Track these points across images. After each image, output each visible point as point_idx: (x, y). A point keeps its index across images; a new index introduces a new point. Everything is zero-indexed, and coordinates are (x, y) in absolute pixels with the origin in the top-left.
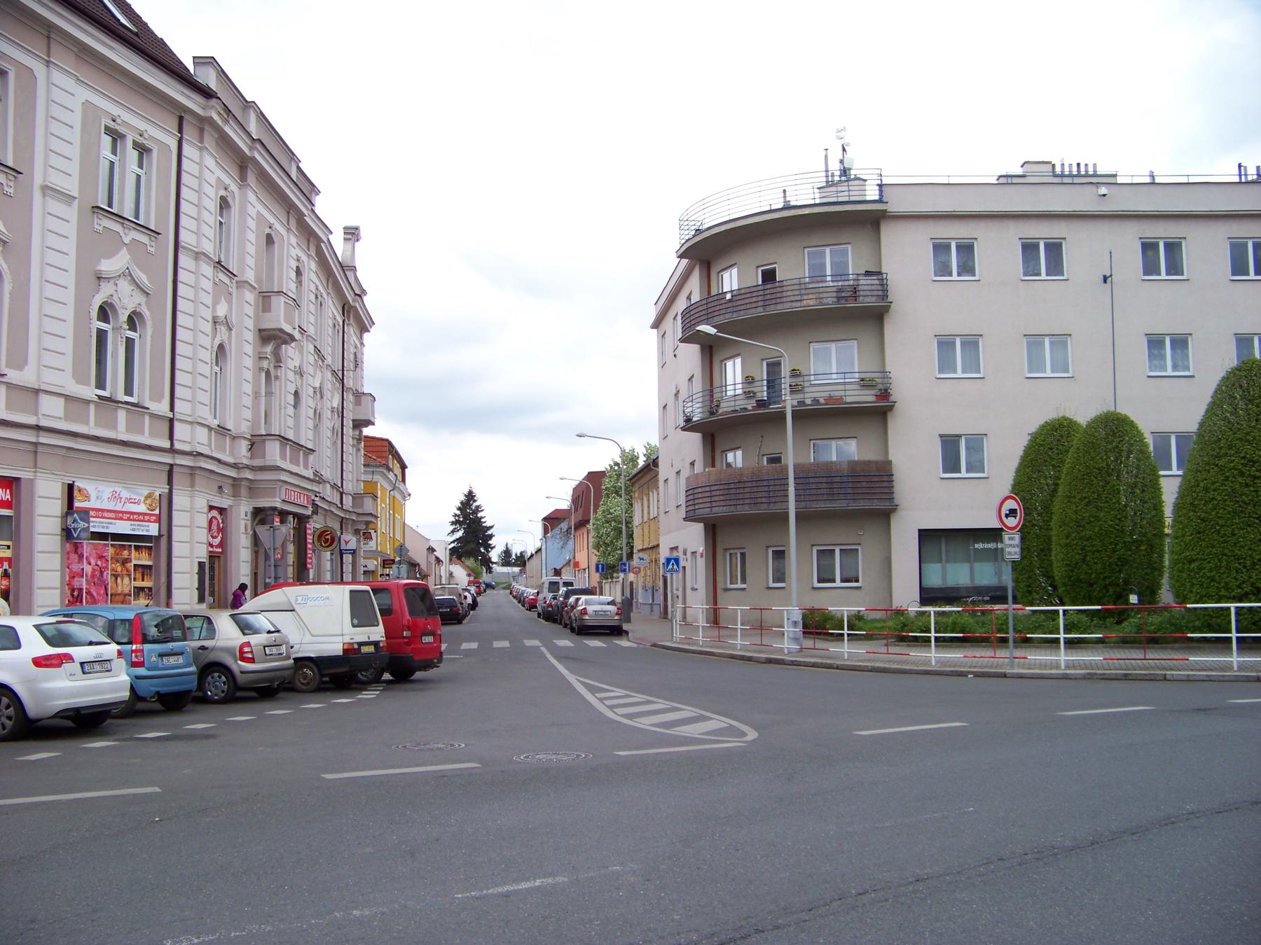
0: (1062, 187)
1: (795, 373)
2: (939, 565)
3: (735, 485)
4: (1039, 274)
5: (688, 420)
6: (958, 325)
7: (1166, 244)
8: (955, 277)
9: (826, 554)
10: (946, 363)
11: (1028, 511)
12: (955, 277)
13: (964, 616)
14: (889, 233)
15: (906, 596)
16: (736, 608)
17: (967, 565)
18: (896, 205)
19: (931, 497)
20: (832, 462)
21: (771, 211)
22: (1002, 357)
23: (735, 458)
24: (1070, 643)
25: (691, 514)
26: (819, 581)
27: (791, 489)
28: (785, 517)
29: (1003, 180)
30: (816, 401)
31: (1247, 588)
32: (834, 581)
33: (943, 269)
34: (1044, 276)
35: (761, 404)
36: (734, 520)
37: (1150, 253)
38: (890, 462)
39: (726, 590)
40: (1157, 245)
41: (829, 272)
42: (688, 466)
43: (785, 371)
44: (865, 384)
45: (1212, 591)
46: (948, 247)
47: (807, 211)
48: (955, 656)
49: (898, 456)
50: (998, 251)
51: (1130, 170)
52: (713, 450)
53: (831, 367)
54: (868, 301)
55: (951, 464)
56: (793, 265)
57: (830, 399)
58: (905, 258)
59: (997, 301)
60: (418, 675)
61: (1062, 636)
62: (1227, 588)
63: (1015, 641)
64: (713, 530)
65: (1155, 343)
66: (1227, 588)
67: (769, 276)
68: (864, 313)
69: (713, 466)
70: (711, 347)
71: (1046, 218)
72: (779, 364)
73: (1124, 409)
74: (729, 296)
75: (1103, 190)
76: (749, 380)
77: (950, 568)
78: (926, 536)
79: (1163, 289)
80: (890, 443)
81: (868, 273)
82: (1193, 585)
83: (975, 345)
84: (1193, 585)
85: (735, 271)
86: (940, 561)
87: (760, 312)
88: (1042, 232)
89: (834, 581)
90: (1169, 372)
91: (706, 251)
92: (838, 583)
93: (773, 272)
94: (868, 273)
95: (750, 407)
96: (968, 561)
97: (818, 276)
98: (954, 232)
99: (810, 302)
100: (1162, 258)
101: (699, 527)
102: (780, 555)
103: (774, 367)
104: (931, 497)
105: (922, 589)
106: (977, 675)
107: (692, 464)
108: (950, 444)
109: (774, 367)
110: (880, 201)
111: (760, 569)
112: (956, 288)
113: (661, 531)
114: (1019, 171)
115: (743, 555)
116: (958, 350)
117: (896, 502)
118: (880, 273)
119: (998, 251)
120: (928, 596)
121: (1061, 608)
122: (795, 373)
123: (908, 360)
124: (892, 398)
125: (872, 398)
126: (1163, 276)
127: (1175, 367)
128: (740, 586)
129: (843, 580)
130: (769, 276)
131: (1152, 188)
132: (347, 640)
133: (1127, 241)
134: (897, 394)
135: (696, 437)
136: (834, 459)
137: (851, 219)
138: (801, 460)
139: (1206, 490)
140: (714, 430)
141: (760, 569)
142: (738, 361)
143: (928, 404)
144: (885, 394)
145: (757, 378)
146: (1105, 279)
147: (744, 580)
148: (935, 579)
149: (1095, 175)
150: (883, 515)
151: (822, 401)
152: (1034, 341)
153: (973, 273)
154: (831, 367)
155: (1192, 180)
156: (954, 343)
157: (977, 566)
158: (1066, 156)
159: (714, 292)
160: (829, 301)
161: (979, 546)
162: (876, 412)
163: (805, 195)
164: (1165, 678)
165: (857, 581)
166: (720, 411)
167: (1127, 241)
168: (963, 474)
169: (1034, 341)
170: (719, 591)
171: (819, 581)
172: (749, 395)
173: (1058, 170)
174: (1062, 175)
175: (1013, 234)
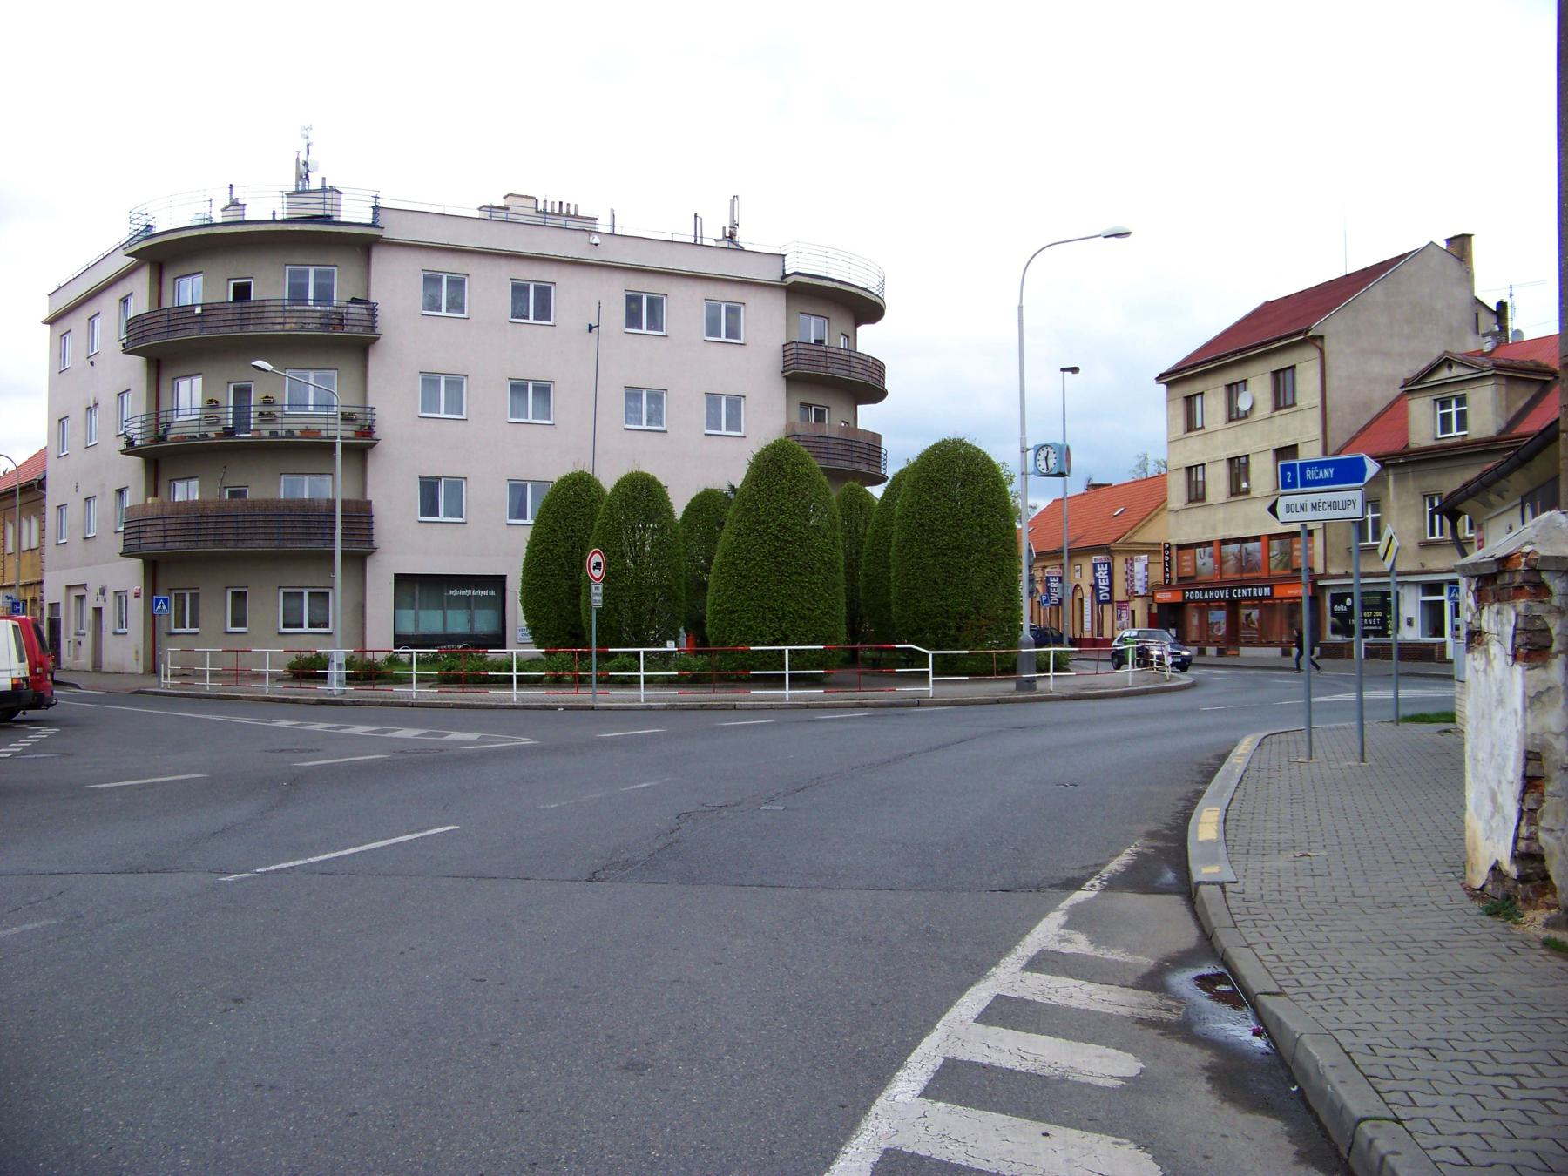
1: (268, 401)
2: (412, 612)
3: (191, 519)
4: (439, 309)
6: (443, 363)
8: (444, 312)
9: (293, 598)
12: (444, 312)
13: (463, 662)
14: (382, 262)
16: (171, 653)
17: (440, 612)
19: (407, 543)
20: (279, 501)
21: (274, 221)
23: (187, 492)
26: (285, 626)
27: (338, 532)
28: (332, 554)
29: (485, 215)
30: (290, 433)
31: (778, 635)
32: (301, 626)
33: (433, 304)
36: (174, 559)
38: (370, 502)
40: (527, 288)
41: (311, 295)
43: (255, 398)
46: (439, 280)
47: (829, 284)
49: (377, 494)
50: (489, 289)
53: (306, 397)
54: (358, 332)
55: (429, 506)
56: (270, 283)
57: (306, 432)
58: (395, 287)
61: (787, 672)
63: (598, 682)
64: (154, 568)
65: (633, 394)
67: (242, 292)
68: (349, 342)
69: (156, 495)
70: (158, 361)
71: (534, 259)
72: (248, 390)
74: (198, 310)
75: (596, 239)
76: (212, 404)
77: (423, 614)
78: (400, 579)
79: (641, 344)
81: (354, 301)
83: (660, 398)
85: (199, 279)
86: (412, 608)
87: (235, 332)
88: (534, 274)
89: (301, 626)
90: (644, 426)
91: (161, 255)
92: (306, 629)
93: (248, 286)
94: (354, 301)
95: (212, 435)
96: (442, 607)
97: (298, 294)
98: (732, 294)
100: (642, 312)
101: (137, 564)
102: (321, 598)
103: (242, 393)
105: (397, 637)
107: (121, 492)
108: (429, 486)
109: (242, 393)
110: (373, 225)
112: (443, 326)
113: (47, 565)
114: (502, 203)
115: (195, 598)
116: (444, 388)
118: (367, 302)
119: (489, 289)
120: (400, 640)
121: (642, 650)
122: (268, 401)
123: (391, 394)
124: (375, 436)
125: (351, 434)
127: (649, 422)
128: (188, 630)
129: (311, 626)
130: (242, 292)
131: (696, 249)
132: (15, 675)
133: (612, 294)
134: (379, 432)
135: (136, 463)
136: (307, 496)
137: (321, 239)
138: (347, 497)
140: (161, 456)
143: (409, 444)
144: (367, 431)
146: (591, 328)
147: (194, 624)
148: (408, 628)
149: (576, 216)
150: (358, 559)
151: (297, 433)
153: (461, 309)
154: (306, 397)
157: (449, 612)
158: (550, 193)
159: (167, 303)
160: (313, 329)
161: (454, 592)
162: (361, 447)
163: (266, 205)
165: (327, 626)
166: (169, 437)
168: (441, 518)
170: (161, 635)
171: (285, 626)
173: (541, 207)
175: (506, 273)
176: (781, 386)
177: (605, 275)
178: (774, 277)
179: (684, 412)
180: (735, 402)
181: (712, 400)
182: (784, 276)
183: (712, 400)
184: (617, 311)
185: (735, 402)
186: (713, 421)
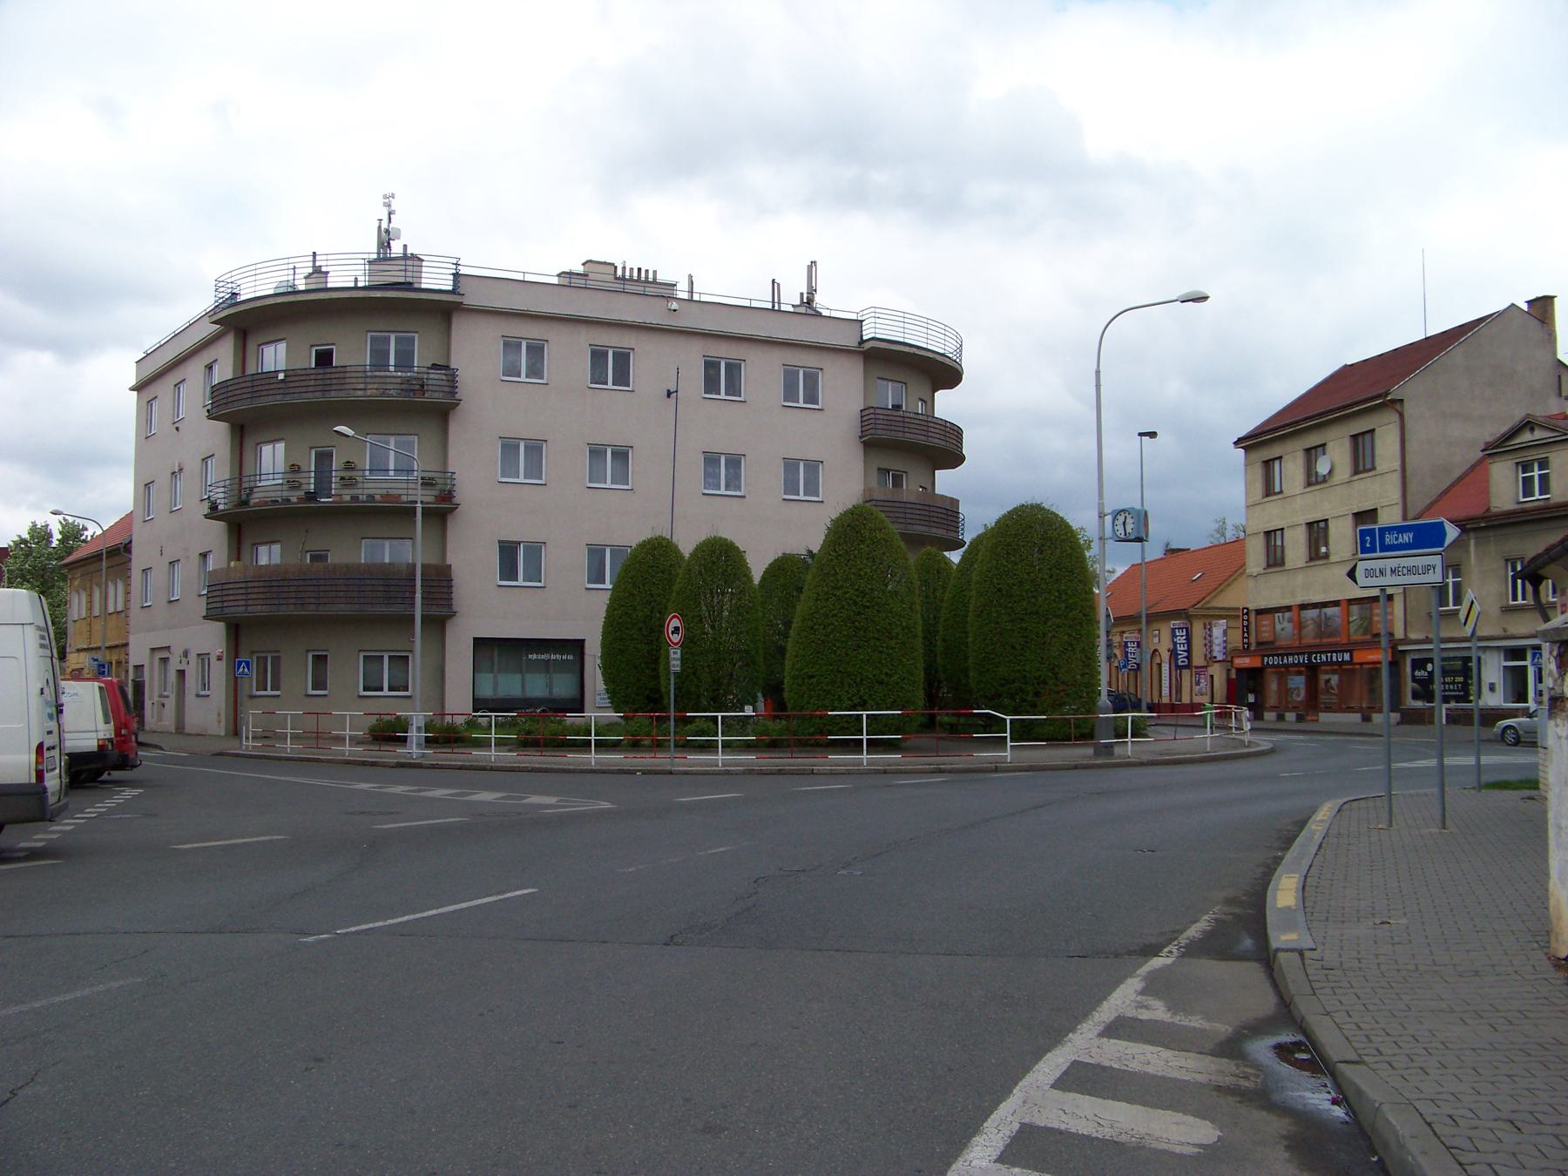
0: (623, 296)
1: (349, 466)
3: (273, 582)
5: (214, 507)
6: (524, 428)
7: (727, 365)
8: (523, 378)
10: (509, 466)
11: (687, 629)
13: (543, 727)
15: (458, 702)
16: (252, 715)
17: (518, 677)
18: (470, 300)
19: (488, 607)
20: (360, 565)
22: (566, 463)
23: (268, 556)
24: (726, 745)
25: (213, 612)
29: (566, 281)
30: (371, 497)
31: (856, 700)
34: (610, 385)
35: (311, 497)
36: (255, 622)
37: (712, 372)
39: (252, 697)
41: (392, 362)
42: (196, 559)
44: (427, 483)
45: (827, 702)
48: (615, 758)
51: (712, 288)
52: (239, 542)
53: (387, 462)
54: (434, 396)
55: (508, 571)
56: (352, 350)
57: (386, 497)
58: (475, 354)
59: (564, 404)
60: (105, 777)
62: (840, 700)
64: (236, 631)
65: (711, 460)
66: (840, 700)
67: (324, 358)
68: (430, 407)
69: (239, 559)
73: (726, 533)
77: (502, 678)
80: (449, 546)
81: (435, 366)
82: (810, 697)
84: (810, 697)
87: (317, 397)
91: (243, 322)
92: (386, 692)
93: (330, 353)
99: (372, 392)
100: (721, 378)
102: (401, 661)
103: (324, 458)
104: (488, 607)
105: (474, 700)
106: (644, 773)
107: (204, 556)
108: (508, 551)
109: (324, 458)
111: (298, 674)
114: (581, 269)
116: (524, 453)
117: (455, 608)
118: (447, 367)
119: (568, 356)
120: (479, 704)
121: (720, 715)
123: (471, 460)
124: (455, 500)
126: (723, 396)
127: (727, 487)
128: (269, 692)
130: (324, 358)
133: (692, 358)
134: (459, 496)
135: (219, 527)
137: (398, 304)
139: (827, 616)
140: (243, 520)
141: (298, 674)
142: (281, 446)
143: (490, 506)
144: (447, 496)
145: (304, 468)
146: (669, 394)
148: (487, 691)
149: (655, 281)
150: (438, 623)
151: (378, 498)
152: (596, 452)
154: (387, 462)
155: (754, 304)
156: (518, 447)
157: (528, 676)
159: (251, 370)
160: (394, 394)
164: (812, 772)
167: (692, 358)
169: (596, 452)
172: (293, 485)
173: (619, 273)
174: (623, 278)
175: (584, 340)
176: (857, 452)
177: (682, 342)
178: (852, 342)
179: (762, 479)
180: (813, 466)
181: (790, 465)
182: (862, 342)
183: (790, 465)
184: (583, 366)
185: (813, 466)
186: (791, 487)
